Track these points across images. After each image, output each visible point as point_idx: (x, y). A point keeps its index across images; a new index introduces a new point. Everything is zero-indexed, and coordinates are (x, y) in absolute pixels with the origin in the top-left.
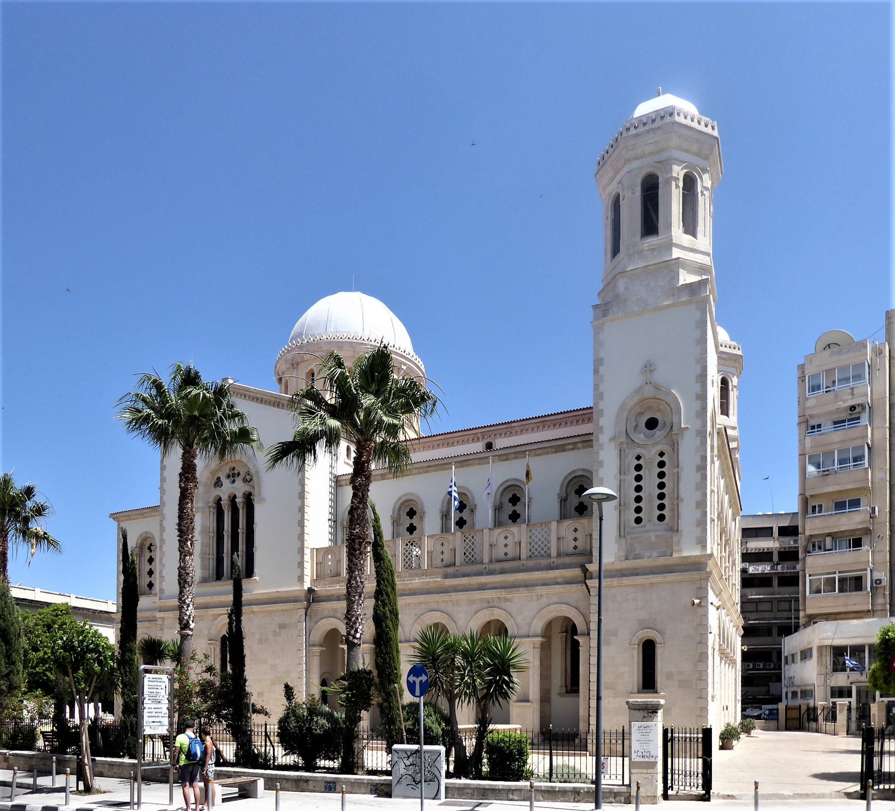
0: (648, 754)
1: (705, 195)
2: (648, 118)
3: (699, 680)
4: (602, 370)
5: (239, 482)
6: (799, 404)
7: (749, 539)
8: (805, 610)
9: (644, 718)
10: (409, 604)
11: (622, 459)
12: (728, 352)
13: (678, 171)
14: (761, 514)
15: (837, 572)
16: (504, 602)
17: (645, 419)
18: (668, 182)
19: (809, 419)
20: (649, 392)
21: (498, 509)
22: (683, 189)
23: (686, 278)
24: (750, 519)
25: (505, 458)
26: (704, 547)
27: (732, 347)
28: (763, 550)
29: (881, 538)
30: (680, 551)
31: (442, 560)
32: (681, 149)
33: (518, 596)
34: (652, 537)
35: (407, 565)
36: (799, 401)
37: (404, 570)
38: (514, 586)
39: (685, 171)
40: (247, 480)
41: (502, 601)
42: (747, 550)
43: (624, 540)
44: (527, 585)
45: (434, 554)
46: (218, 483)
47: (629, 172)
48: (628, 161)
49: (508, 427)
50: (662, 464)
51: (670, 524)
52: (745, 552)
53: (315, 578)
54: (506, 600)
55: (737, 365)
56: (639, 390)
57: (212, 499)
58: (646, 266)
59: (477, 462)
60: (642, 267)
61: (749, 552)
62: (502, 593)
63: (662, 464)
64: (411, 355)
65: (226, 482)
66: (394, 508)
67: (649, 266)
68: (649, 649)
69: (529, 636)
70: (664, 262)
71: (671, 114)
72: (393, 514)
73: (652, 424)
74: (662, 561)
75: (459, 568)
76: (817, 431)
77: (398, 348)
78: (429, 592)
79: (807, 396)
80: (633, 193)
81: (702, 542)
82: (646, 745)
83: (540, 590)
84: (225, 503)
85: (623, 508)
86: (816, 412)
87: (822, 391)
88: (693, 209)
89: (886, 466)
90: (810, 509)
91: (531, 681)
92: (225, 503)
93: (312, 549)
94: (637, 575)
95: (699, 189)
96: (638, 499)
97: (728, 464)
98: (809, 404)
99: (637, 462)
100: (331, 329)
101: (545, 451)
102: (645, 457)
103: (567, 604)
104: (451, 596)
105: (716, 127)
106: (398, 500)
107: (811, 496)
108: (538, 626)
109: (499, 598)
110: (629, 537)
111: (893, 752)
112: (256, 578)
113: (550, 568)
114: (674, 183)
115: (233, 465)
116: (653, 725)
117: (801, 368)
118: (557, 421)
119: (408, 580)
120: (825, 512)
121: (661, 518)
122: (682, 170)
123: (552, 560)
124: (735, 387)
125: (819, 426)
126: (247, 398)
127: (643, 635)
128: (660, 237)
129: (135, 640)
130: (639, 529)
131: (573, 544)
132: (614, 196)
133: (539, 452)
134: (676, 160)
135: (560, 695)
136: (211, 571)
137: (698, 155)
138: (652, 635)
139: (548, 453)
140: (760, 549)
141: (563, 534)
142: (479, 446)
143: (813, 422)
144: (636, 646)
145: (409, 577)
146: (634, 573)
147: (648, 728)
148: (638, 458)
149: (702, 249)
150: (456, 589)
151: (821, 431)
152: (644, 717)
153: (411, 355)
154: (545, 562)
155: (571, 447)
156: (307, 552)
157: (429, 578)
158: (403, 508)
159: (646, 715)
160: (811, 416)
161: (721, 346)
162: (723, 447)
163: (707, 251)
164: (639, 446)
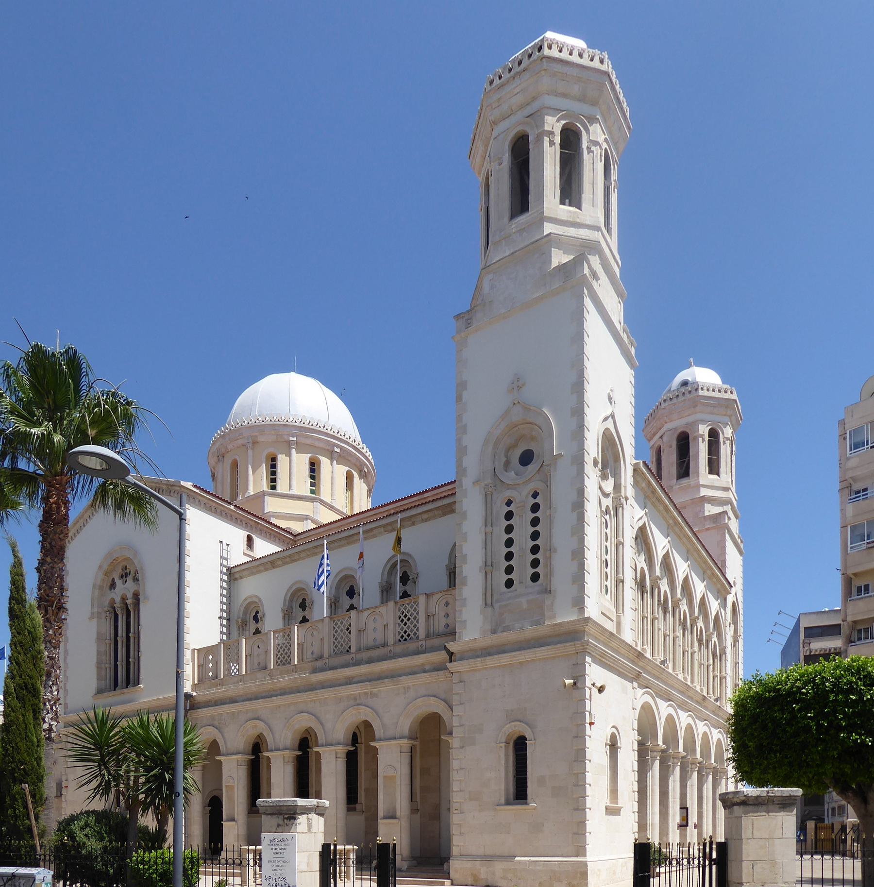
0: (283, 883)
1: (593, 152)
3: (574, 785)
4: (465, 395)
6: (840, 468)
7: (812, 640)
9: (279, 828)
10: (279, 706)
11: (489, 505)
12: (717, 396)
13: (554, 124)
14: (827, 610)
16: (371, 698)
17: (518, 452)
19: (852, 482)
22: (562, 146)
24: (814, 616)
26: (582, 609)
27: (723, 391)
28: (830, 650)
30: (554, 617)
31: (312, 653)
32: (557, 94)
33: (385, 688)
34: (524, 602)
35: (279, 661)
36: (840, 464)
37: (276, 667)
38: (380, 677)
39: (564, 122)
41: (369, 697)
42: (811, 652)
43: (490, 609)
44: (393, 676)
45: (305, 646)
47: (496, 138)
48: (494, 123)
50: (535, 508)
51: (544, 584)
52: (808, 654)
53: (196, 682)
54: (373, 695)
55: (729, 412)
56: (507, 412)
57: (107, 603)
58: (513, 253)
60: (509, 255)
61: (812, 654)
62: (366, 688)
63: (535, 508)
64: (357, 443)
65: (119, 582)
66: (285, 600)
67: (516, 251)
68: (520, 746)
69: (395, 739)
70: (533, 243)
72: (284, 605)
73: (526, 458)
74: (529, 632)
75: (327, 661)
77: (343, 434)
78: (297, 691)
80: (500, 164)
81: (579, 603)
82: (281, 868)
83: (406, 681)
85: (489, 569)
86: (859, 473)
87: (866, 447)
90: (854, 590)
91: (398, 793)
93: (193, 650)
94: (504, 652)
96: (509, 556)
97: (674, 519)
98: (852, 463)
101: (431, 514)
103: (435, 696)
104: (316, 694)
106: (288, 590)
107: (855, 575)
108: (405, 725)
109: (366, 694)
110: (497, 606)
111: (858, 881)
112: (141, 685)
113: (417, 652)
115: (124, 564)
116: (289, 839)
117: (842, 423)
119: (278, 678)
120: (872, 592)
121: (535, 577)
122: (558, 121)
123: (420, 643)
124: (728, 439)
125: (866, 490)
127: (511, 731)
130: (510, 594)
133: (425, 516)
134: (550, 108)
137: (582, 99)
138: (520, 729)
139: (434, 517)
140: (826, 650)
141: (432, 610)
143: (857, 487)
144: (503, 745)
145: (280, 674)
146: (501, 650)
147: (283, 843)
148: (509, 503)
149: (588, 222)
150: (323, 686)
151: (867, 494)
152: (279, 825)
153: (357, 443)
156: (188, 655)
157: (299, 674)
158: (295, 599)
159: (281, 822)
160: (854, 479)
161: (702, 389)
162: (652, 492)
163: (595, 224)
164: (509, 487)
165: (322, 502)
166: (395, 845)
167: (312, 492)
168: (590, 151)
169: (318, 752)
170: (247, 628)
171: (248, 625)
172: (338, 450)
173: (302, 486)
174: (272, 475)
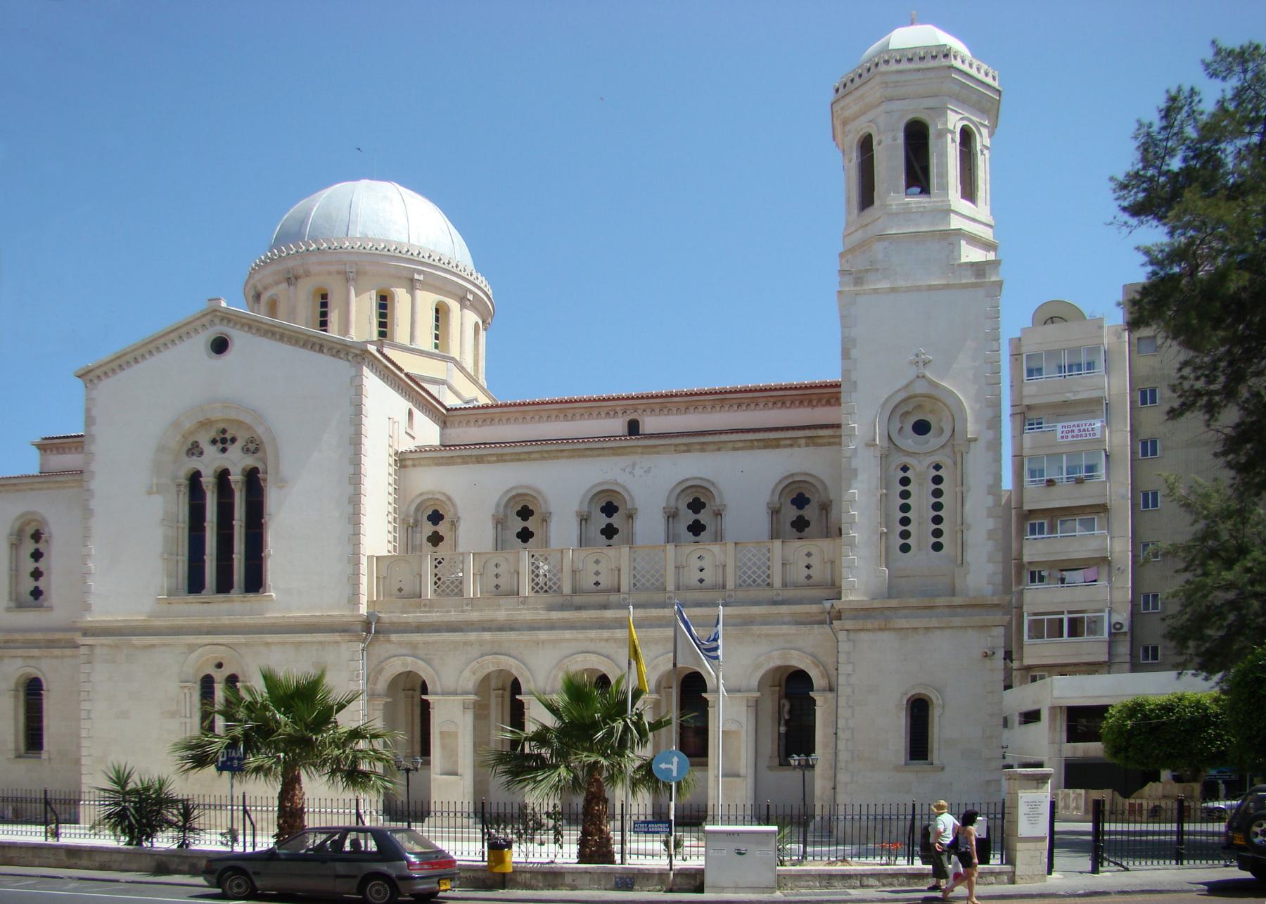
2: (915, 54)
4: (854, 353)
5: (235, 451)
8: (1021, 660)
15: (1066, 612)
18: (942, 134)
20: (920, 388)
21: (671, 515)
23: (970, 254)
25: (686, 448)
29: (1121, 571)
37: (532, 594)
40: (248, 450)
46: (195, 450)
49: (665, 401)
59: (640, 450)
65: (211, 451)
71: (946, 56)
72: (497, 512)
76: (1038, 428)
77: (437, 259)
79: (1025, 381)
84: (208, 481)
88: (970, 169)
89: (1127, 480)
92: (208, 481)
93: (370, 558)
95: (979, 147)
99: (903, 474)
100: (356, 232)
102: (915, 470)
105: (997, 78)
114: (949, 136)
118: (743, 401)
126: (254, 331)
128: (932, 200)
129: (610, 682)
131: (806, 572)
132: (861, 137)
135: (770, 768)
136: (180, 577)
142: (617, 425)
148: (905, 469)
151: (1041, 428)
154: (768, 594)
155: (788, 442)
156: (364, 560)
165: (452, 359)
166: (1104, 801)
167: (436, 346)
168: (982, 152)
169: (427, 700)
170: (419, 529)
171: (419, 526)
172: (421, 278)
173: (425, 340)
174: (322, 299)
